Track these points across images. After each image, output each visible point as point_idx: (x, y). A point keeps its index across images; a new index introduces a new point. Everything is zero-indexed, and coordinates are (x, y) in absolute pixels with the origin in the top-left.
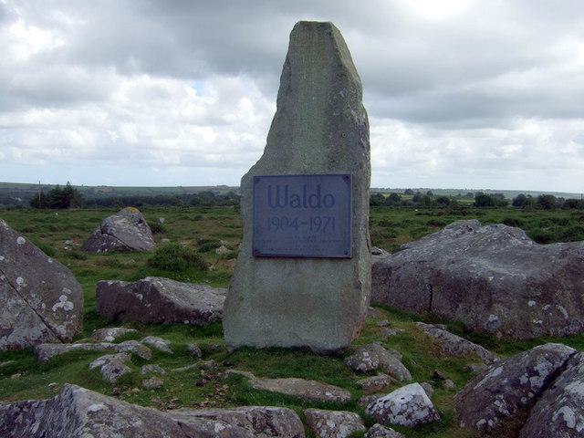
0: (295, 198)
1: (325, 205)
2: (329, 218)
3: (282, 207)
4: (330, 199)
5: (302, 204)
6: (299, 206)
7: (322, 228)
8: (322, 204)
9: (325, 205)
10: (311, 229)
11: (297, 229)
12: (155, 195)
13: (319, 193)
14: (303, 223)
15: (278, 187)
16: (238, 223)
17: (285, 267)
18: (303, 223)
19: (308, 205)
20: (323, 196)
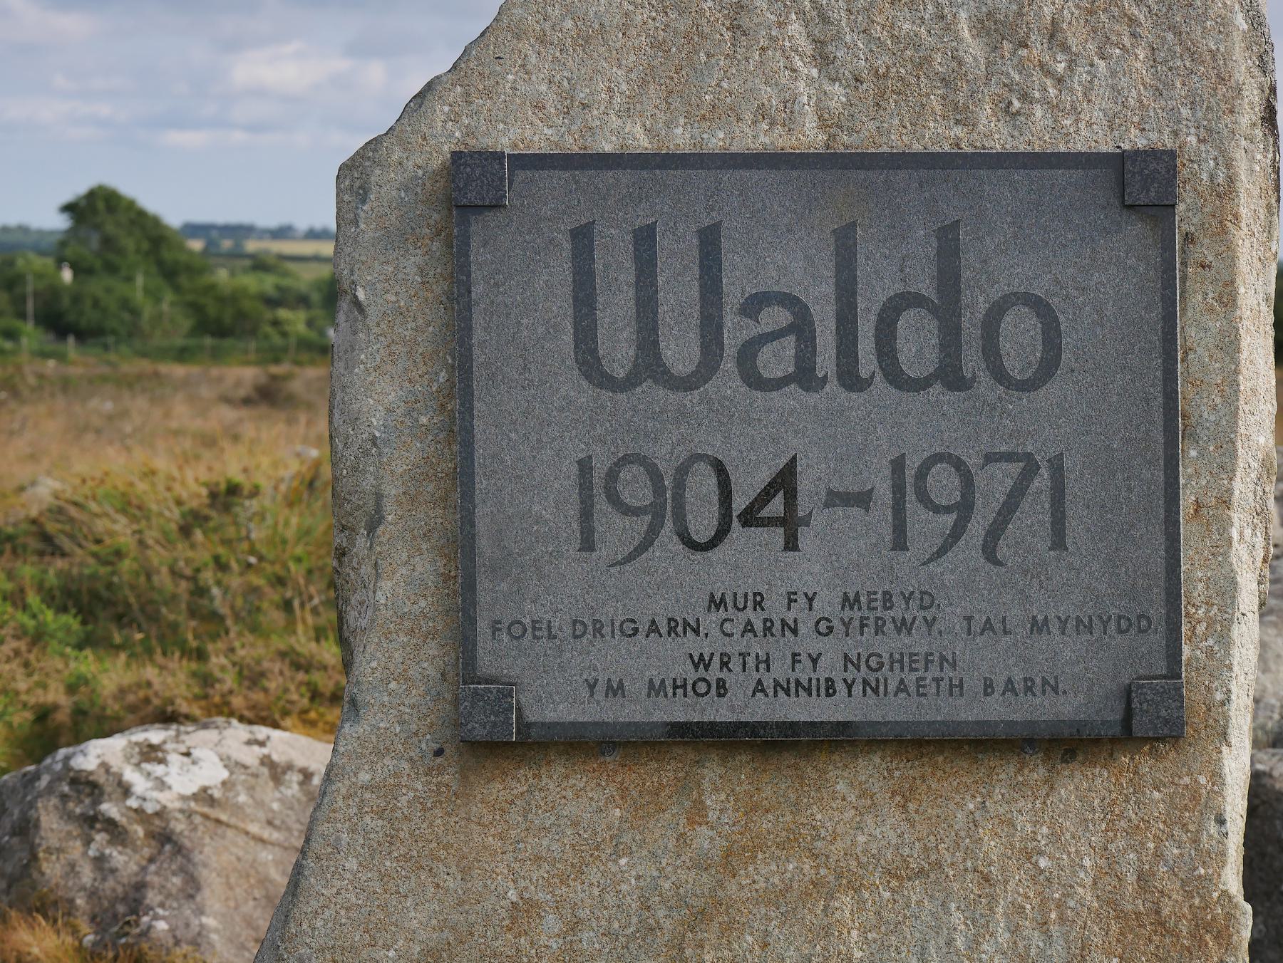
0: (777, 317)
1: (1000, 375)
2: (1031, 468)
3: (686, 384)
4: (1013, 366)
5: (826, 361)
6: (805, 376)
7: (977, 528)
8: (972, 362)
9: (1000, 375)
10: (900, 543)
11: (791, 544)
12: (836, 757)
13: (949, 280)
14: (836, 499)
15: (735, 594)
16: (612, 570)
17: (697, 814)
18: (836, 499)
19: (867, 362)
20: (976, 305)
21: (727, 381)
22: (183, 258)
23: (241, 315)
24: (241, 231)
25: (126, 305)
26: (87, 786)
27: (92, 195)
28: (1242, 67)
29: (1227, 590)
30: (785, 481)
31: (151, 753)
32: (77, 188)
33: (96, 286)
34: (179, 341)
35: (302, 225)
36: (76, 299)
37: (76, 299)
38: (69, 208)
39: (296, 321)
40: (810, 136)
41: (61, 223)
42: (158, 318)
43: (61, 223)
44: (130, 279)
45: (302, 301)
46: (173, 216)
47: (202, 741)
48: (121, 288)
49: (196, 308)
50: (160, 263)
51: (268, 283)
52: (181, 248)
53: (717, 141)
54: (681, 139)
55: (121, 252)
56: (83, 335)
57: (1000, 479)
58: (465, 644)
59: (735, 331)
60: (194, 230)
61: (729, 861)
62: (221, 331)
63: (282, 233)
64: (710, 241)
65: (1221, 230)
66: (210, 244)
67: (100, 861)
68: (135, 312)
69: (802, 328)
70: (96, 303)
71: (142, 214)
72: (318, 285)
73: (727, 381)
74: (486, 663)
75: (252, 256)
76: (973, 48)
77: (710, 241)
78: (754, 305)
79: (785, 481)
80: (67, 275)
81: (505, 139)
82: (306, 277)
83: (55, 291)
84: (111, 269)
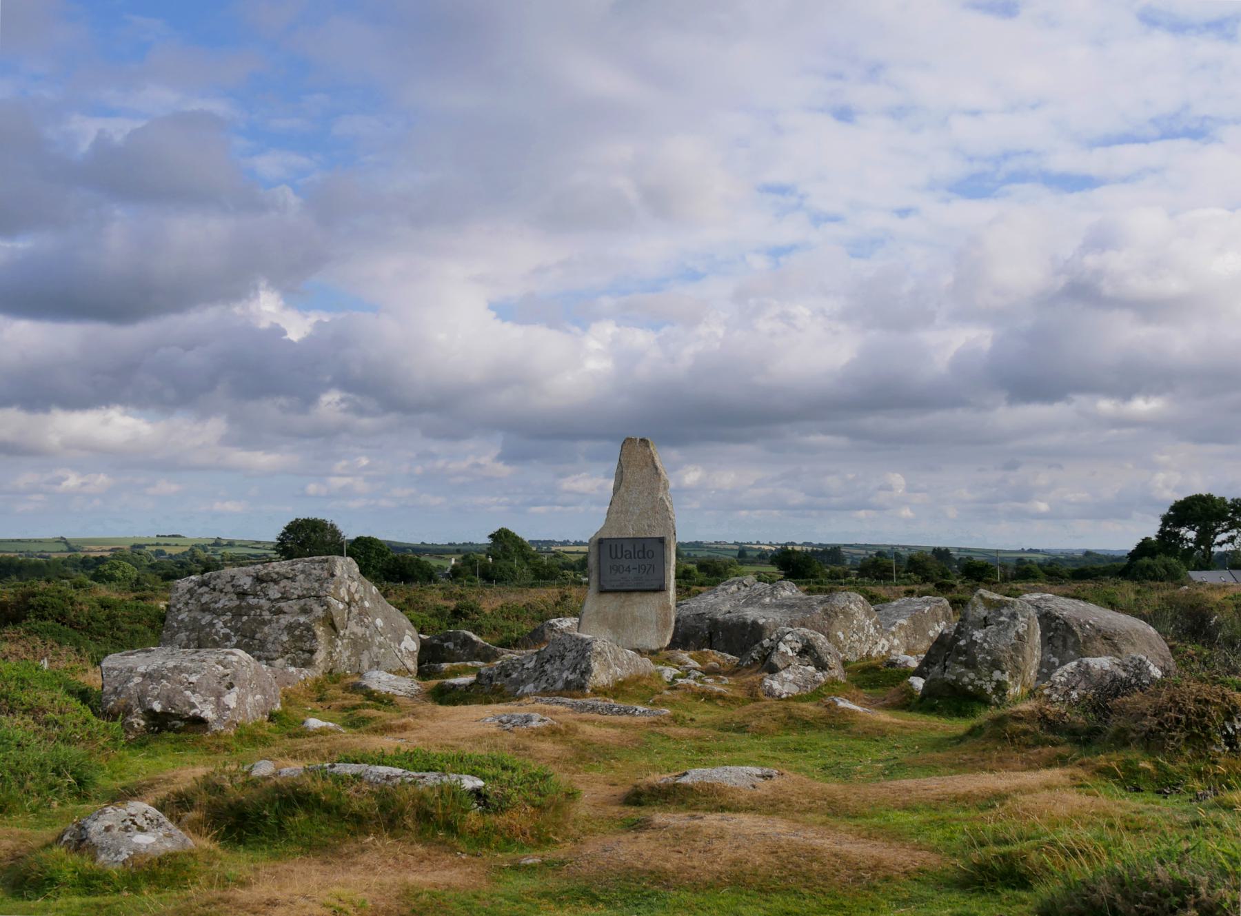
20: (646, 550)
21: (624, 558)
22: (531, 553)
23: (551, 572)
24: (549, 543)
25: (511, 570)
26: (551, 625)
27: (500, 531)
28: (671, 529)
29: (670, 577)
30: (629, 567)
31: (560, 621)
32: (495, 529)
33: (501, 563)
34: (530, 581)
35: (572, 540)
36: (494, 568)
37: (494, 568)
38: (491, 536)
39: (570, 574)
40: (632, 536)
41: (489, 541)
42: (522, 575)
43: (489, 541)
44: (513, 561)
45: (572, 568)
46: (526, 539)
47: (567, 619)
48: (509, 563)
49: (535, 571)
50: (523, 555)
51: (560, 561)
52: (531, 549)
53: (623, 537)
54: (620, 536)
55: (509, 551)
56: (499, 580)
57: (648, 567)
58: (600, 582)
59: (624, 554)
60: (533, 542)
61: (624, 602)
62: (545, 578)
63: (565, 543)
64: (622, 546)
65: (670, 545)
66: (539, 547)
67: (554, 636)
68: (514, 572)
69: (630, 553)
70: (500, 569)
71: (517, 537)
72: (578, 562)
73: (624, 558)
74: (602, 583)
75: (553, 552)
76: (647, 528)
77: (622, 546)
78: (626, 551)
79: (629, 567)
80: (490, 559)
81: (604, 537)
82: (574, 558)
83: (487, 565)
84: (506, 557)
